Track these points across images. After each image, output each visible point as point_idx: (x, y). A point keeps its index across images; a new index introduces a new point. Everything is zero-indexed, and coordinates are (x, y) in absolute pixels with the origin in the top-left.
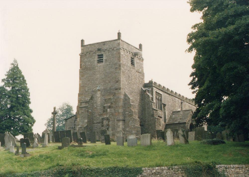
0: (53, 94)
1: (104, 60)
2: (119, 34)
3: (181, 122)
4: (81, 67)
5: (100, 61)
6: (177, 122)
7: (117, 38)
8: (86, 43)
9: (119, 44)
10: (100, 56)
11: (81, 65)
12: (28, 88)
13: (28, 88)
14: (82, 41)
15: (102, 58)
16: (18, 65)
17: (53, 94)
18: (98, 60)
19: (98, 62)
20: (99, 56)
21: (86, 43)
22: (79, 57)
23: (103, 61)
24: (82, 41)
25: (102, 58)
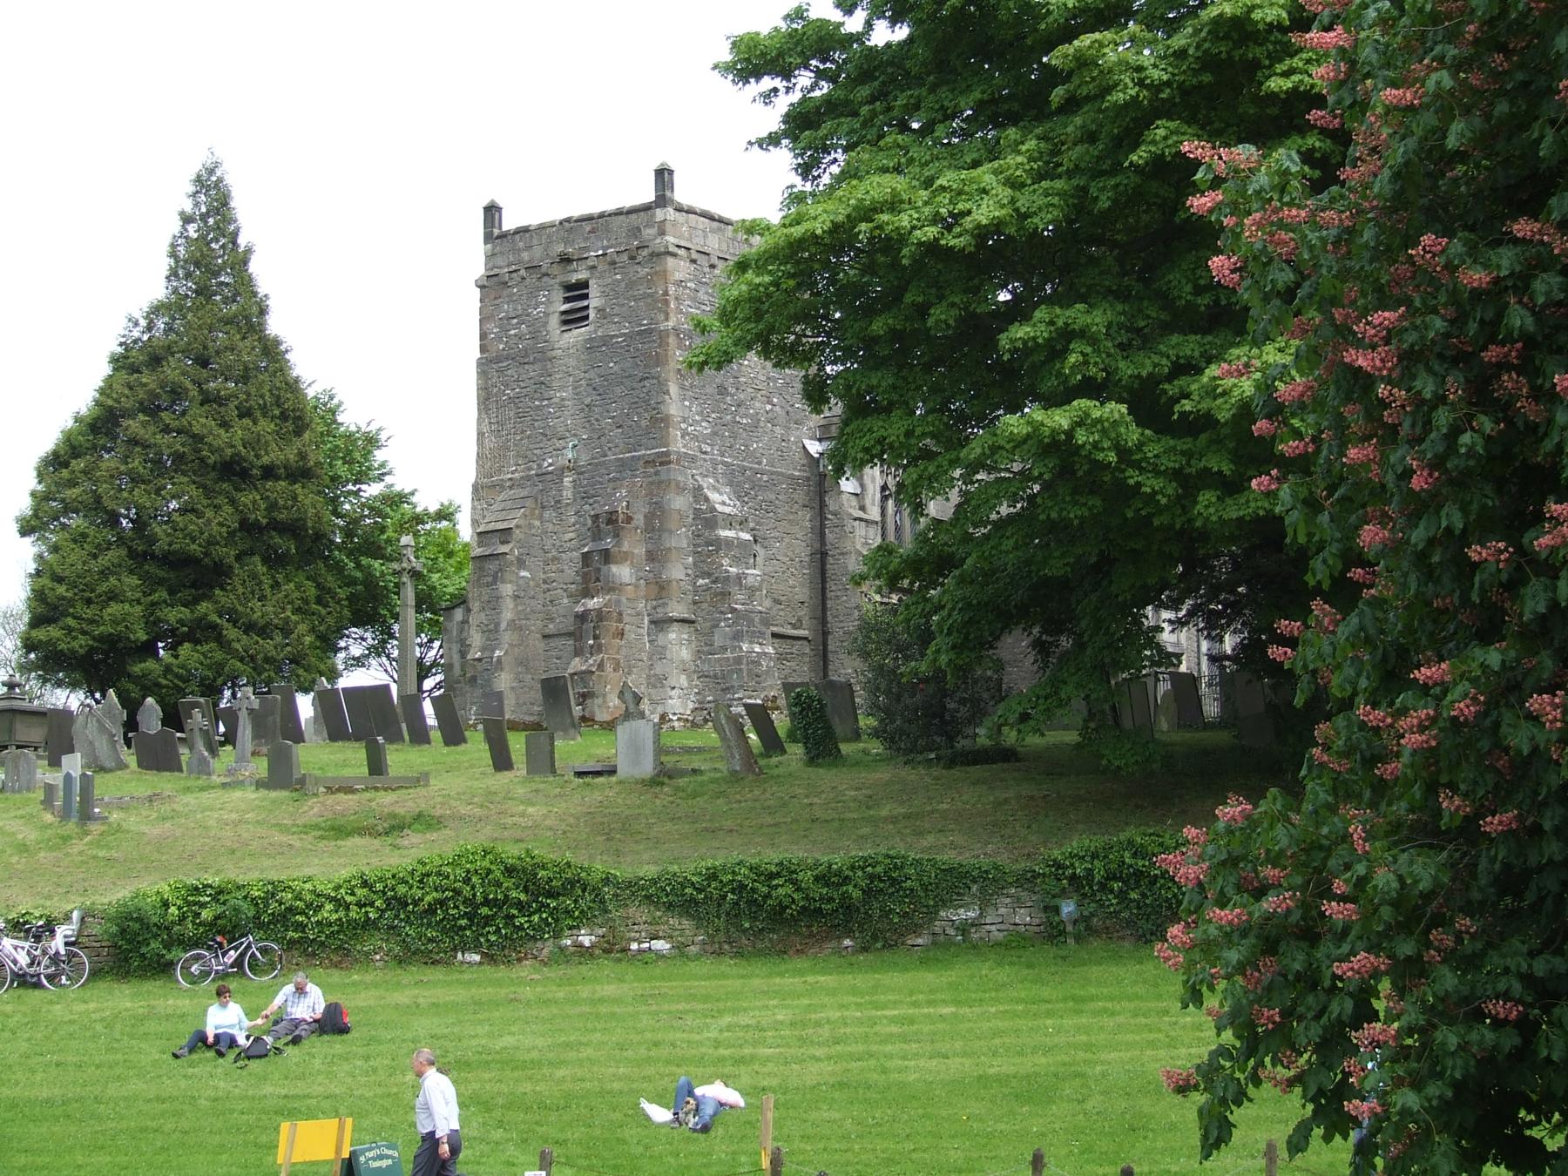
1: (592, 314)
2: (663, 176)
4: (483, 349)
5: (573, 319)
10: (577, 291)
11: (483, 336)
14: (492, 212)
15: (585, 303)
18: (586, 297)
19: (565, 322)
22: (476, 293)
23: (587, 317)
24: (492, 212)
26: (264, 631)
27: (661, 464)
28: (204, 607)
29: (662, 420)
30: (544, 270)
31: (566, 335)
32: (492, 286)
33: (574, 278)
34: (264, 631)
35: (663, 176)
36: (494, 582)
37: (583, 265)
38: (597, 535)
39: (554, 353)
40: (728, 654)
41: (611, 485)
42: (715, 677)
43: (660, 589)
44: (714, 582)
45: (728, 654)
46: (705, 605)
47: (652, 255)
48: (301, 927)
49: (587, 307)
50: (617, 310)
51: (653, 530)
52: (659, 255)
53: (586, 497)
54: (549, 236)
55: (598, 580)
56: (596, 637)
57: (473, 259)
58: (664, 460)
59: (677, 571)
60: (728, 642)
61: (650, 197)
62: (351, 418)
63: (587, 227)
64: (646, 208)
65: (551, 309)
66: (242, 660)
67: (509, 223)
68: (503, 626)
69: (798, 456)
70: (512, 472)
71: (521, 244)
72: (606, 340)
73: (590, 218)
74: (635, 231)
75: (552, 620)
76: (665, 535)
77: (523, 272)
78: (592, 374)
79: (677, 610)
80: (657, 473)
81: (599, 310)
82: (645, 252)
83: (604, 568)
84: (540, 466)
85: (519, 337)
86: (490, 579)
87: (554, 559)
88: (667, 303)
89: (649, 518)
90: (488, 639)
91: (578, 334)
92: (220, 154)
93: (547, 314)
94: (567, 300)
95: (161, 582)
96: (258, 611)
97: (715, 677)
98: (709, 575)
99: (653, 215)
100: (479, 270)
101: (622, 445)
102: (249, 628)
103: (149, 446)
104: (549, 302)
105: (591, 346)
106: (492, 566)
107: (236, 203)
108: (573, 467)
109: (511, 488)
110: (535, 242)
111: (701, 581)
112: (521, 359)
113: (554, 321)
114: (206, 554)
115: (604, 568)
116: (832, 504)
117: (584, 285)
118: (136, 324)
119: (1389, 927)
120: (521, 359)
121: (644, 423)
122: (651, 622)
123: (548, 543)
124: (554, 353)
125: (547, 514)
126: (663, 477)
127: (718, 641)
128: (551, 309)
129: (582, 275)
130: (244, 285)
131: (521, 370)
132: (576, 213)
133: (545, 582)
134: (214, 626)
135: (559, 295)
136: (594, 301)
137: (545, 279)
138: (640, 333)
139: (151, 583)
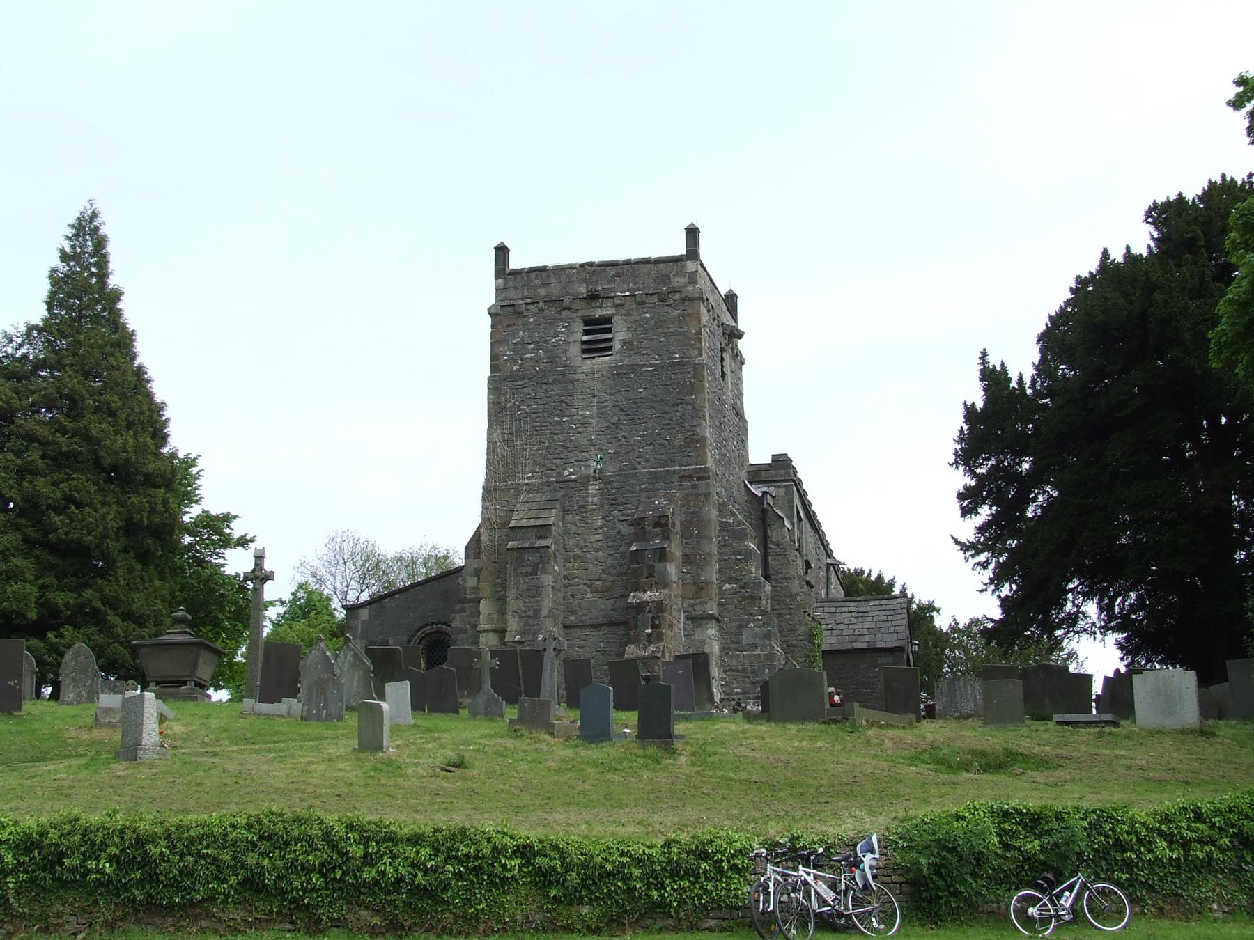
0: (336, 446)
1: (617, 346)
2: (692, 234)
3: (879, 645)
4: (494, 368)
5: (590, 349)
6: (864, 646)
7: (680, 249)
8: (516, 262)
9: (693, 278)
10: (599, 326)
11: (494, 357)
12: (1142, 240)
13: (1142, 240)
14: (502, 252)
15: (610, 336)
16: (122, 273)
17: (336, 446)
18: (609, 331)
19: (584, 351)
20: (587, 322)
21: (516, 262)
22: (488, 320)
23: (610, 348)
24: (502, 252)
25: (610, 336)
26: (140, 621)
27: (698, 479)
28: (88, 594)
29: (698, 441)
30: (565, 304)
31: (588, 362)
32: (504, 317)
33: (598, 313)
34: (140, 621)
35: (692, 234)
36: (535, 570)
37: (609, 303)
38: (641, 536)
39: (576, 376)
40: (758, 651)
41: (644, 494)
42: (744, 671)
43: (698, 589)
44: (742, 587)
45: (758, 651)
46: (732, 607)
47: (683, 300)
48: (1129, 865)
49: (611, 340)
50: (645, 343)
51: (691, 536)
52: (691, 300)
53: (615, 503)
54: (568, 277)
55: (651, 575)
56: (654, 627)
58: (704, 476)
59: (712, 574)
60: (758, 641)
61: (680, 249)
65: (572, 339)
66: (121, 644)
67: (515, 263)
68: (544, 612)
69: (742, 497)
70: (528, 476)
71: (537, 282)
72: (634, 369)
73: (614, 264)
74: (665, 279)
75: (573, 612)
76: (705, 541)
77: (541, 304)
78: (619, 397)
79: (713, 609)
80: (693, 487)
81: (624, 342)
82: (677, 296)
83: (658, 566)
84: (559, 474)
85: (537, 361)
86: (529, 570)
87: (576, 557)
88: (700, 340)
89: (686, 526)
90: (527, 624)
91: (599, 363)
92: (100, 207)
93: (566, 343)
94: (586, 333)
95: (52, 567)
96: (138, 601)
97: (744, 671)
98: (736, 581)
99: (683, 267)
100: (490, 299)
101: (652, 461)
102: (127, 616)
103: (46, 443)
104: (569, 331)
105: (617, 373)
106: (531, 558)
107: (110, 248)
108: (599, 476)
109: (528, 492)
110: (553, 280)
111: (727, 586)
112: (540, 379)
113: (575, 349)
114: (98, 546)
115: (658, 566)
116: (774, 536)
117: (609, 320)
118: (11, 341)
120: (540, 379)
121: (677, 442)
122: (688, 618)
123: (571, 543)
124: (576, 376)
125: (569, 517)
126: (702, 490)
127: (746, 639)
128: (572, 339)
129: (608, 311)
130: (115, 322)
131: (538, 389)
132: (597, 258)
133: (566, 577)
134: (95, 611)
135: (579, 327)
136: (620, 334)
137: (566, 312)
138: (672, 364)
139: (43, 569)
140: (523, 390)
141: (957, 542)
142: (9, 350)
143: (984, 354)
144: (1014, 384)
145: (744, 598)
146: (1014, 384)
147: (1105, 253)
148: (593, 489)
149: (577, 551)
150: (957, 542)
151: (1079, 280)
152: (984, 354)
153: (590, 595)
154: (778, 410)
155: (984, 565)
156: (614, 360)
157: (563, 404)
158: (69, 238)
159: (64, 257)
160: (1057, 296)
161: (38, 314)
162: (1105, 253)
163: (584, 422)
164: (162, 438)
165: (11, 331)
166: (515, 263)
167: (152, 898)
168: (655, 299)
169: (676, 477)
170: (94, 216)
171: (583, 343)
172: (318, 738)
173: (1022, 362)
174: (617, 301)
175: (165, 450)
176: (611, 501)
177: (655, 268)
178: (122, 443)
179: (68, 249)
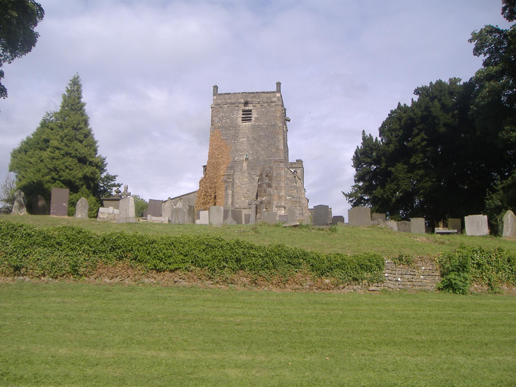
1: (253, 119)
2: (279, 84)
5: (244, 120)
7: (275, 89)
11: (212, 121)
14: (216, 88)
16: (87, 97)
18: (251, 114)
19: (242, 120)
23: (251, 120)
24: (216, 88)
32: (216, 108)
33: (247, 108)
35: (279, 84)
37: (251, 105)
49: (251, 117)
56: (266, 208)
57: (210, 100)
61: (275, 89)
62: (395, 107)
63: (252, 95)
64: (274, 92)
65: (238, 116)
67: (219, 92)
72: (259, 126)
82: (274, 104)
91: (247, 124)
94: (243, 114)
98: (291, 196)
105: (253, 127)
110: (232, 97)
117: (251, 111)
119: (13, 266)
128: (238, 116)
136: (254, 115)
138: (272, 126)
140: (221, 134)
141: (344, 193)
142: (48, 118)
143: (364, 132)
144: (374, 141)
145: (293, 201)
146: (374, 141)
147: (399, 103)
148: (245, 164)
149: (239, 184)
150: (344, 193)
151: (392, 111)
152: (364, 132)
153: (243, 199)
154: (298, 146)
155: (351, 201)
156: (250, 126)
157: (235, 136)
158: (69, 84)
159: (68, 91)
160: (384, 117)
161: (58, 109)
162: (399, 103)
163: (242, 143)
164: (95, 151)
165: (49, 112)
166: (219, 92)
167: (31, 237)
168: (266, 105)
169: (273, 161)
170: (78, 77)
171: (242, 118)
172: (35, 297)
173: (375, 135)
174: (254, 105)
175: (97, 156)
176: (251, 167)
177: (266, 95)
178: (84, 151)
179: (69, 88)
